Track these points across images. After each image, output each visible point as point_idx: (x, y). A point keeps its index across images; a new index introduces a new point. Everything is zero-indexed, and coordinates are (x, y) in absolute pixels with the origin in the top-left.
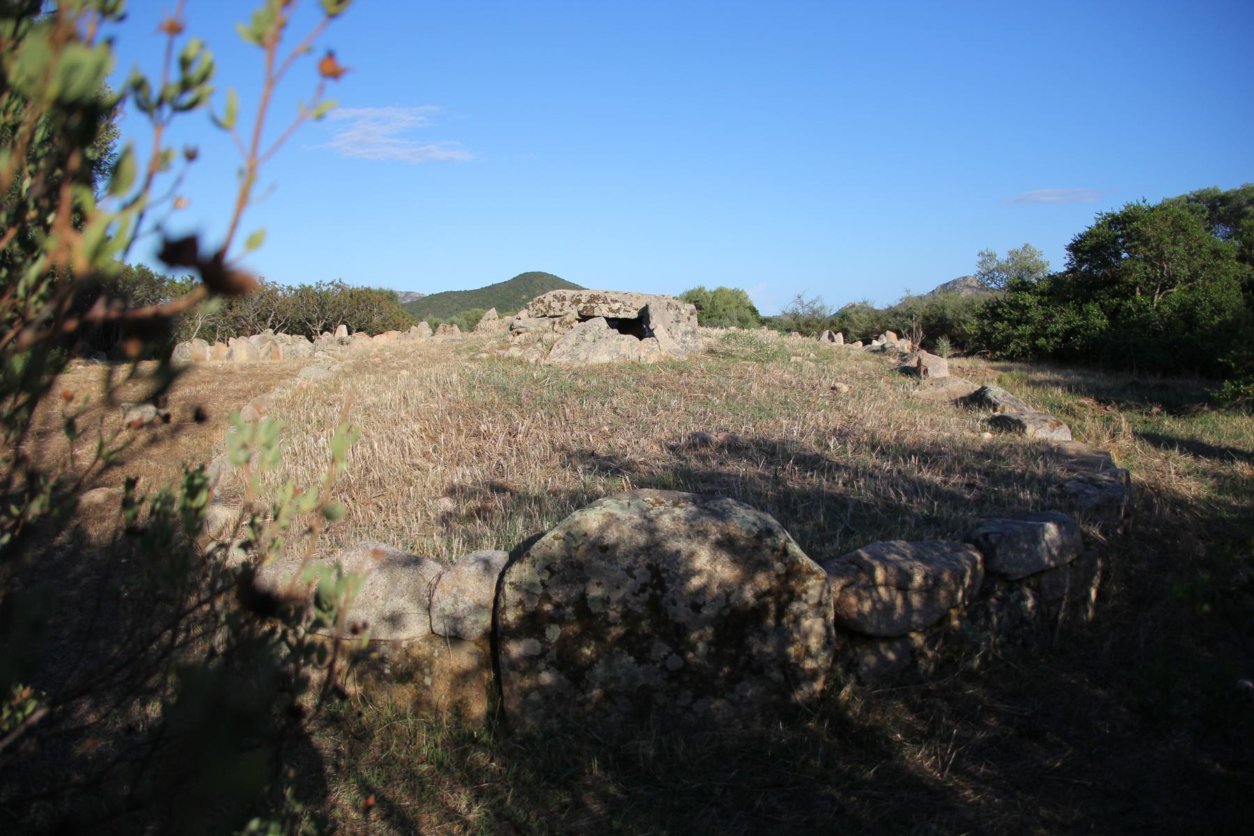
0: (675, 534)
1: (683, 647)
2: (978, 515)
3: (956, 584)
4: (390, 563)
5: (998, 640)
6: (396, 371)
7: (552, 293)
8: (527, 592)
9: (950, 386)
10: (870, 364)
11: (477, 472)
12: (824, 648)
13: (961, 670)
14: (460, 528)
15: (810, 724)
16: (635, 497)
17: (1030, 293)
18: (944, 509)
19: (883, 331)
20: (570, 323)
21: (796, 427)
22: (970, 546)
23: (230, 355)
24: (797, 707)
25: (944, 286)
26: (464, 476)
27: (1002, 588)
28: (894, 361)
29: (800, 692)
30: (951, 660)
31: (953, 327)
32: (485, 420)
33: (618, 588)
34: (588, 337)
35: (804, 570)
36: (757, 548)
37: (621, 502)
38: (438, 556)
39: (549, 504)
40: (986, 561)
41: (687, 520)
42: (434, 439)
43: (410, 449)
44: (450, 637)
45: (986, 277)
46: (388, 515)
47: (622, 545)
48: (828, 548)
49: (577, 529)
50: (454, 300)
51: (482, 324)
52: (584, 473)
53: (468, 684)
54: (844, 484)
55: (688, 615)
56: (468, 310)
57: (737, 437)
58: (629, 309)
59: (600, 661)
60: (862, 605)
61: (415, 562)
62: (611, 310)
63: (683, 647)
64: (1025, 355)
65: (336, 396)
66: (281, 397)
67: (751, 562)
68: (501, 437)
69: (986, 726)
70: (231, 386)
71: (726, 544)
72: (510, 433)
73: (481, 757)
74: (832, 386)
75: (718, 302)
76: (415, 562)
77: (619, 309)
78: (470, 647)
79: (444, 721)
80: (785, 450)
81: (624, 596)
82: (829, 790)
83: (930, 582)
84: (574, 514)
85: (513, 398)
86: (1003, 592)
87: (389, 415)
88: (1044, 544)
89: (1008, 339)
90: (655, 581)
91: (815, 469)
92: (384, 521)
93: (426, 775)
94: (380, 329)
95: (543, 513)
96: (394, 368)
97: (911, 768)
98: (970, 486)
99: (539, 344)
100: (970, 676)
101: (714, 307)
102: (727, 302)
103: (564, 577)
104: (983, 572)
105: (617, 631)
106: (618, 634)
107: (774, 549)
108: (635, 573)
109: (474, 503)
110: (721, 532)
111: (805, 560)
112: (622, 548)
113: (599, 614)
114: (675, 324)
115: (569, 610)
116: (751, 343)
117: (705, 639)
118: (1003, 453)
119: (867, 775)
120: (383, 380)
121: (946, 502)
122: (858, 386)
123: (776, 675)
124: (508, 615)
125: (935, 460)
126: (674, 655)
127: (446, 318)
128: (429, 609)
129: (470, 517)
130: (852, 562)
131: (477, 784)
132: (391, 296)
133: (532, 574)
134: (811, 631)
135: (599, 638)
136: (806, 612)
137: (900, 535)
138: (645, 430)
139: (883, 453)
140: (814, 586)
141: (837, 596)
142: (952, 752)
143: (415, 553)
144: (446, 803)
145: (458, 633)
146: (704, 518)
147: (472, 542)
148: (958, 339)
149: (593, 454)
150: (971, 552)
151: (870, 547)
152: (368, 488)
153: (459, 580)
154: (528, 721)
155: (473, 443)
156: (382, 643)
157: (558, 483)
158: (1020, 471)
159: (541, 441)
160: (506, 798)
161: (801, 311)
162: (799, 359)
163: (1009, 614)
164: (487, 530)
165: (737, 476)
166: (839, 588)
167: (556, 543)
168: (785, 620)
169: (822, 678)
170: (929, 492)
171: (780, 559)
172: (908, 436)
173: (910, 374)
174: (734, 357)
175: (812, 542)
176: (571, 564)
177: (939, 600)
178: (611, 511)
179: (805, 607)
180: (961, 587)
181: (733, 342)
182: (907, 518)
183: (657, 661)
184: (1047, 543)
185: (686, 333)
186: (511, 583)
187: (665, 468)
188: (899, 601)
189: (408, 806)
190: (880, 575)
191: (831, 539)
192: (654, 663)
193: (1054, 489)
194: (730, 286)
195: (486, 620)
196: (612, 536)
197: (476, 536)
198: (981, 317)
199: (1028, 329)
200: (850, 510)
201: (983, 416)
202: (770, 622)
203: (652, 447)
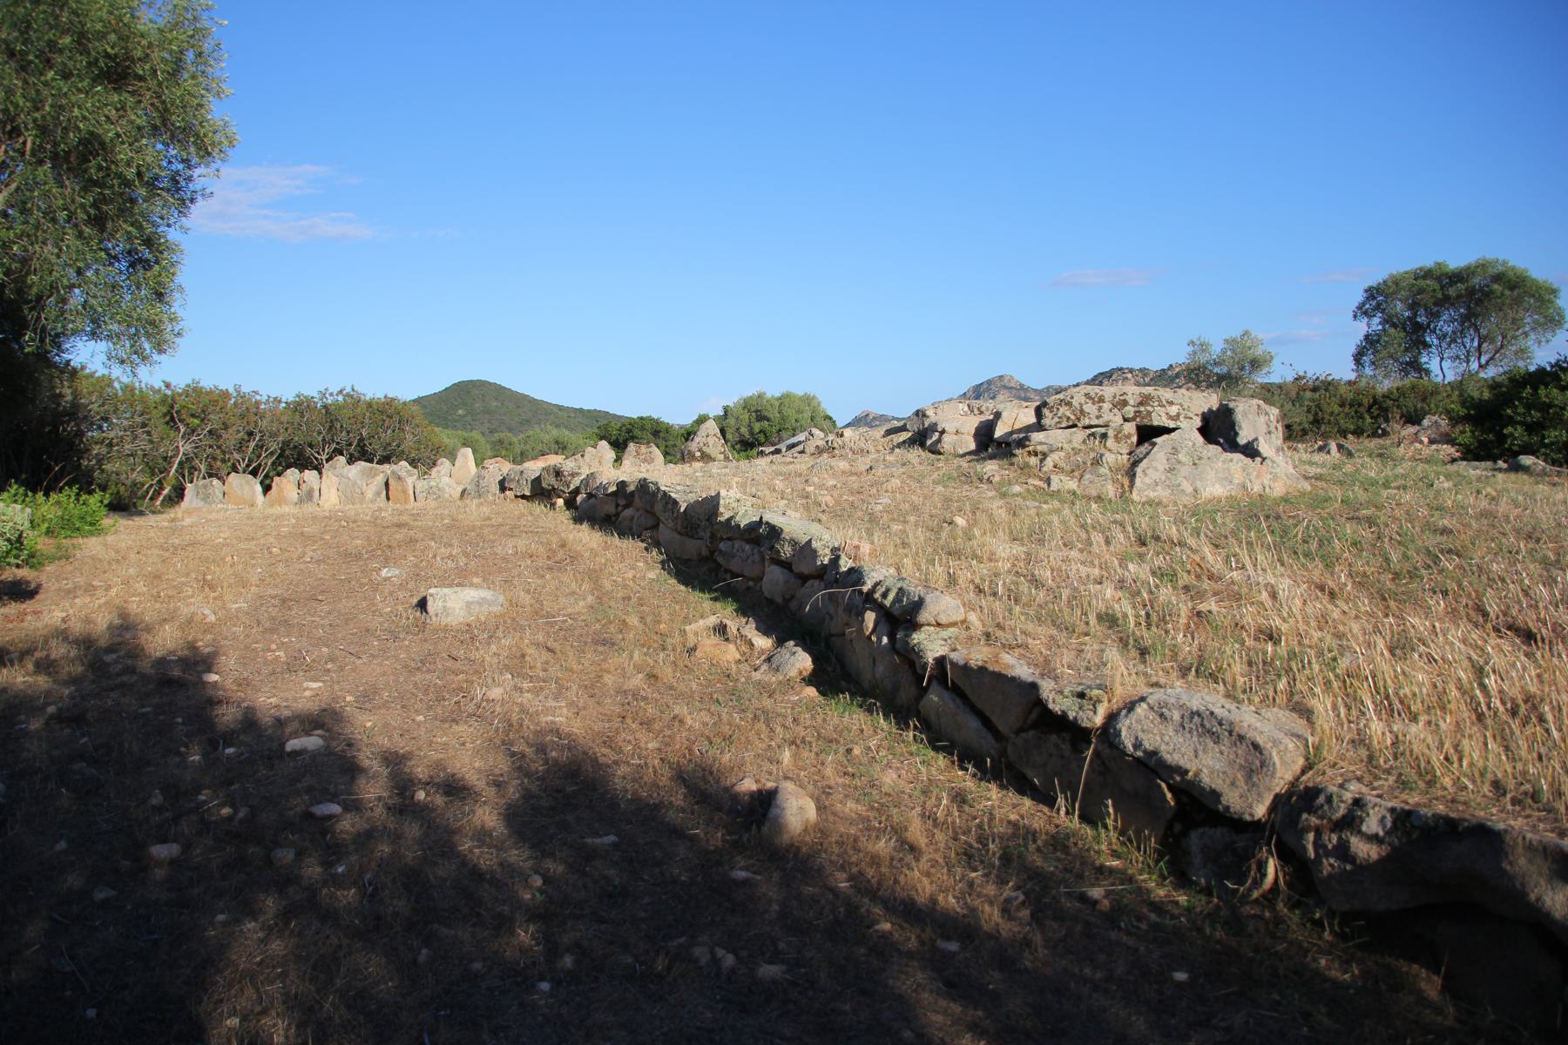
75: (787, 411)
77: (1178, 415)
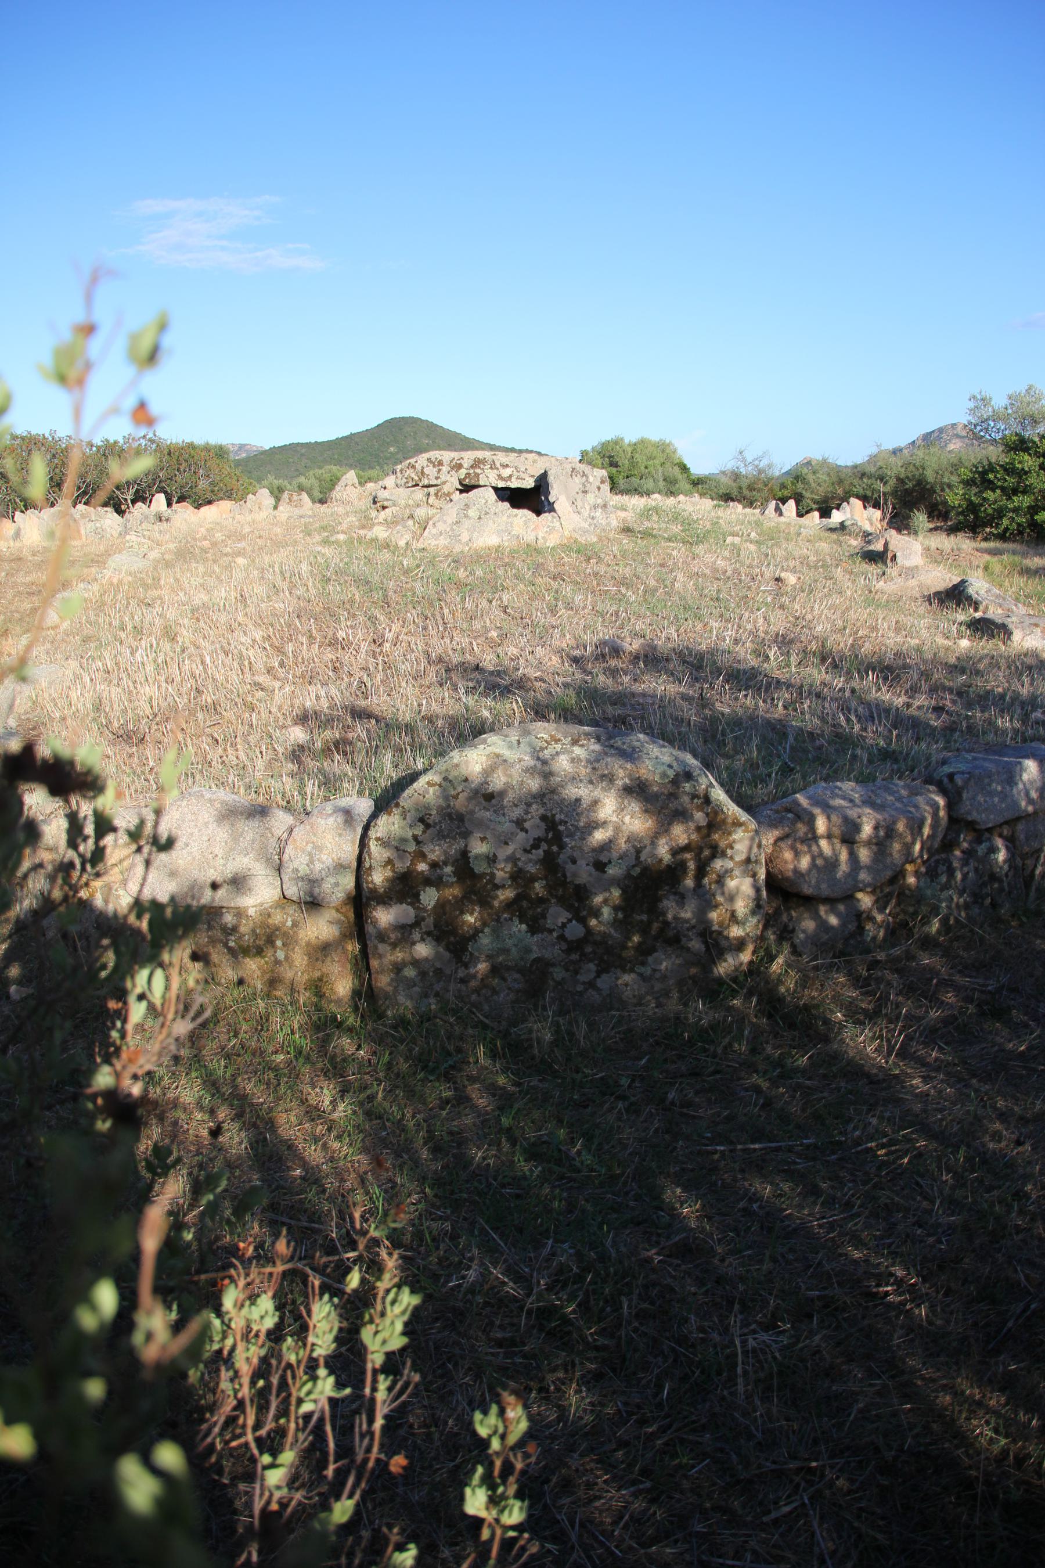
0: (574, 778)
1: (585, 913)
2: (945, 748)
3: (912, 834)
4: (229, 814)
5: (962, 900)
6: (230, 558)
7: (426, 456)
8: (397, 849)
9: (922, 578)
10: (824, 546)
11: (334, 691)
12: (753, 913)
13: (916, 936)
14: (311, 764)
15: (735, 1002)
16: (526, 733)
17: (1030, 455)
18: (904, 739)
19: (845, 499)
20: (449, 494)
21: (730, 633)
22: (932, 788)
23: (17, 535)
24: (720, 981)
25: (927, 437)
26: (318, 698)
27: (968, 838)
28: (855, 543)
29: (724, 964)
30: (904, 925)
31: (935, 492)
32: (343, 625)
33: (506, 843)
34: (472, 513)
35: (730, 820)
36: (673, 796)
37: (508, 739)
38: (288, 802)
39: (423, 735)
40: (950, 806)
41: (588, 761)
42: (280, 650)
43: (250, 663)
44: (306, 903)
45: (979, 428)
46: (225, 750)
47: (510, 792)
48: (761, 792)
49: (456, 773)
50: (302, 455)
51: (337, 493)
52: (467, 692)
53: (329, 959)
54: (785, 707)
55: (590, 875)
56: (320, 468)
57: (656, 646)
58: (522, 475)
59: (486, 930)
60: (799, 861)
61: (260, 812)
62: (500, 477)
63: (585, 913)
64: (1021, 533)
65: (155, 593)
66: (86, 595)
67: (666, 811)
68: (364, 647)
69: (942, 1002)
70: (21, 578)
71: (637, 790)
72: (374, 641)
73: (346, 1044)
74: (777, 576)
75: (638, 457)
76: (260, 812)
77: (511, 476)
78: (330, 914)
79: (301, 1002)
80: (715, 663)
81: (513, 853)
82: (756, 1079)
83: (882, 833)
84: (452, 754)
85: (377, 595)
86: (970, 843)
87: (223, 618)
88: (1021, 786)
89: (1000, 513)
90: (550, 835)
91: (750, 687)
92: (221, 757)
93: (282, 1066)
94: (209, 496)
95: (417, 747)
96: (226, 555)
97: (851, 1053)
98: (938, 710)
99: (410, 522)
100: (927, 943)
101: (633, 464)
102: (651, 458)
103: (440, 831)
104: (946, 819)
105: (506, 894)
106: (507, 899)
107: (694, 796)
108: (527, 825)
109: (331, 734)
110: (630, 776)
111: (732, 809)
112: (511, 796)
113: (483, 875)
114: (581, 495)
115: (448, 869)
116: (676, 518)
117: (611, 903)
118: (981, 666)
119: (800, 1062)
120: (214, 572)
121: (907, 730)
122: (809, 576)
123: (696, 945)
124: (375, 877)
125: (898, 676)
126: (574, 922)
127: (292, 478)
128: (279, 869)
129: (327, 751)
130: (789, 810)
131: (342, 1076)
132: (220, 452)
133: (403, 828)
134: (738, 892)
135: (484, 902)
136: (732, 870)
137: (849, 774)
138: (543, 635)
139: (835, 666)
140: (741, 840)
141: (769, 851)
142: (900, 1034)
143: (261, 799)
144: (307, 1100)
145: (315, 898)
146: (609, 759)
147: (330, 784)
148: (940, 507)
149: (477, 668)
150: (933, 796)
151: (811, 790)
152: (200, 715)
153: (315, 835)
154: (401, 999)
155: (329, 655)
156: (224, 910)
157: (435, 707)
158: (1000, 690)
159: (413, 651)
160: (377, 1093)
161: (743, 471)
162: (737, 540)
163: (976, 870)
164: (348, 769)
165: (654, 696)
166: (771, 841)
167: (431, 790)
168: (706, 881)
169: (750, 948)
170: (887, 717)
171: (700, 808)
172: (867, 644)
173: (875, 561)
174: (654, 537)
175: (742, 783)
176: (450, 815)
177: (891, 855)
178: (497, 751)
179: (730, 864)
180: (919, 839)
181: (655, 518)
182: (859, 752)
183: (554, 930)
184: (1024, 785)
185: (595, 507)
186: (378, 839)
187: (566, 685)
188: (844, 856)
189: (262, 1104)
190: (821, 825)
191: (764, 780)
192: (551, 931)
193: (1039, 715)
194: (654, 437)
195: (348, 882)
196: (498, 781)
197: (334, 776)
198: (968, 483)
199: (1026, 501)
200: (791, 739)
201: (961, 617)
202: (689, 882)
203: (550, 659)
